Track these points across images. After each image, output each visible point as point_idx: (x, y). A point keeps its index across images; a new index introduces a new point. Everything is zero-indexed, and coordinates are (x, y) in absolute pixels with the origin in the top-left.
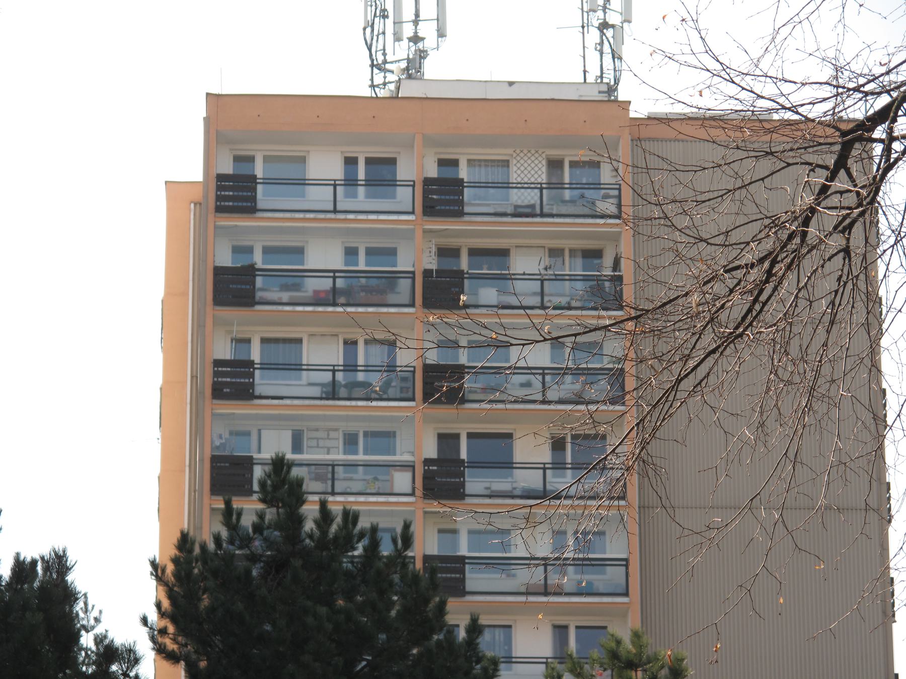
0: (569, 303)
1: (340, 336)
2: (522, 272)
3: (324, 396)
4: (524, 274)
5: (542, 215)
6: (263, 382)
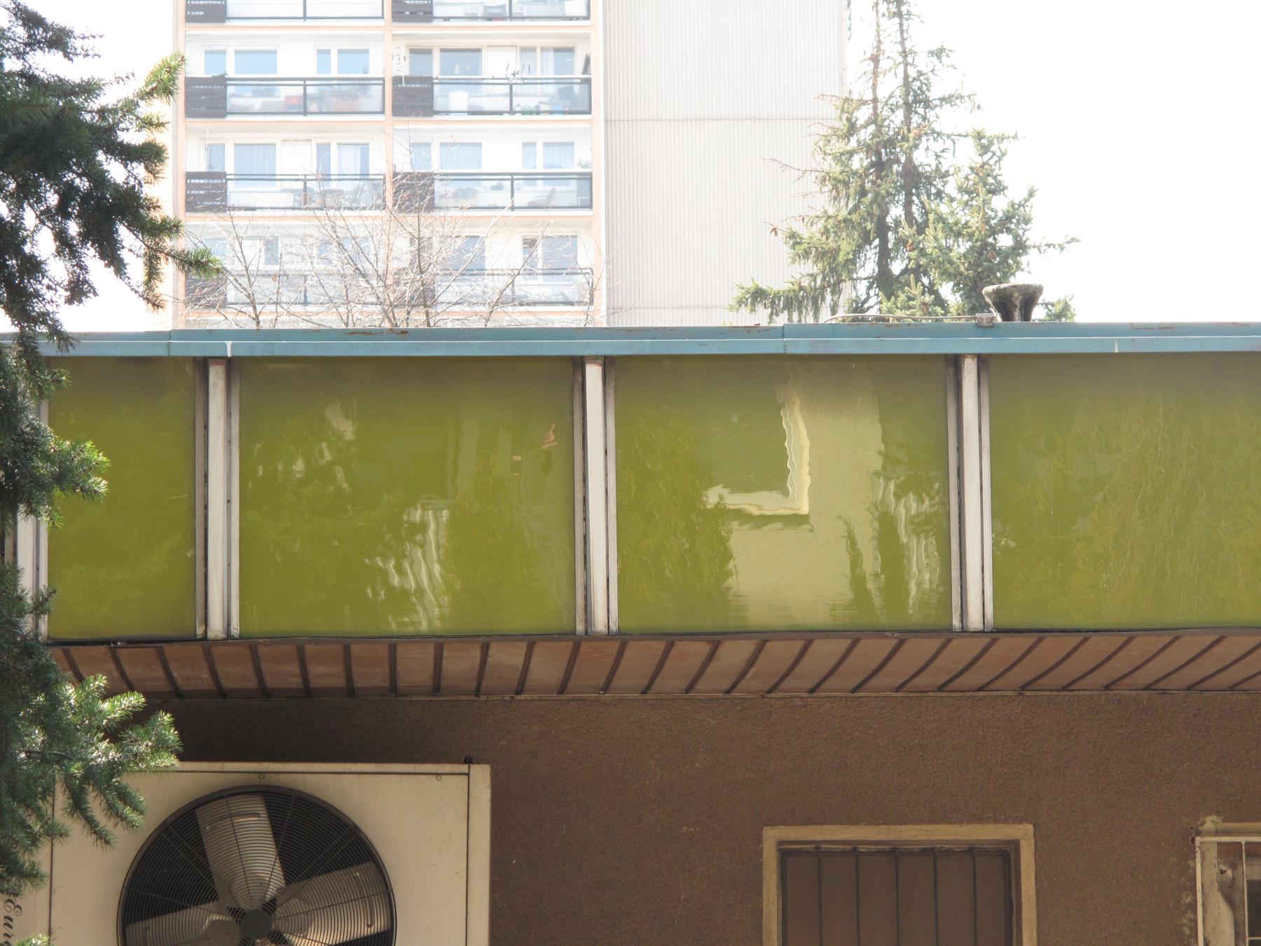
0: (537, 107)
1: (313, 141)
2: (491, 77)
3: (297, 206)
4: (493, 79)
5: (511, 17)
6: (237, 193)
